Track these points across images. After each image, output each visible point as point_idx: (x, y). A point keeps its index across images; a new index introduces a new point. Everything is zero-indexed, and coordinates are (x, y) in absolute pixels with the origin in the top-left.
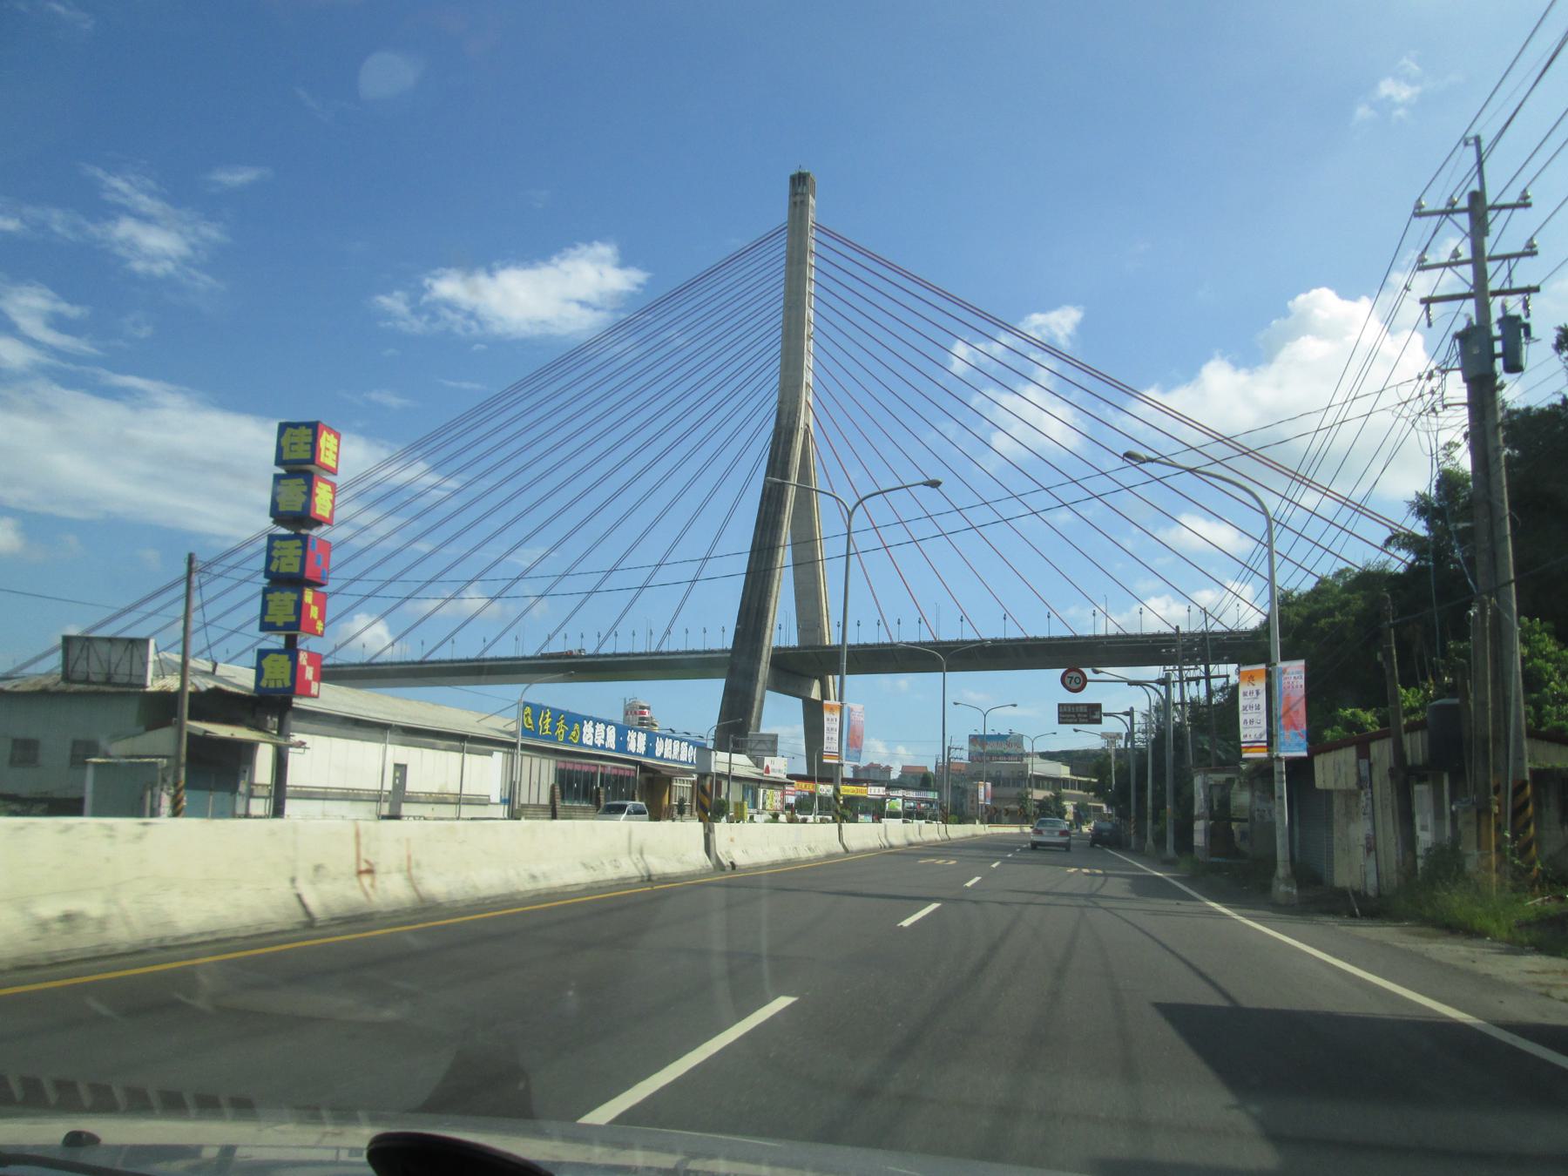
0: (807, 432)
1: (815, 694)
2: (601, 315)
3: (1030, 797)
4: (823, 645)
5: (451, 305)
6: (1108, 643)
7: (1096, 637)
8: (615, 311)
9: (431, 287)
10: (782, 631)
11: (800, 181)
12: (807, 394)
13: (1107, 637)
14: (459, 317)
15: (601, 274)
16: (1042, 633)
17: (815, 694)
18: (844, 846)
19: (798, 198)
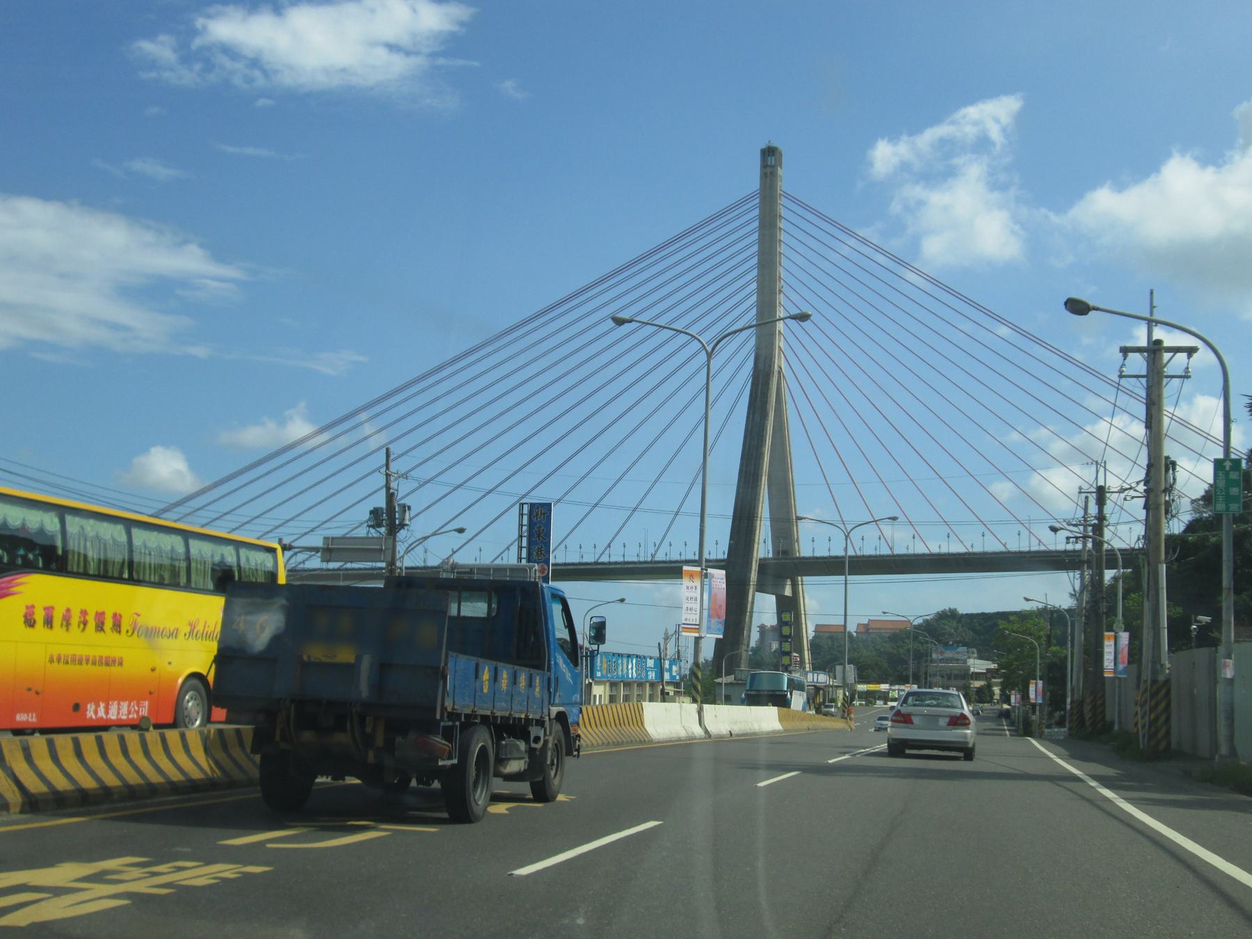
0: (779, 373)
1: (788, 592)
2: (414, 61)
3: (972, 686)
4: (794, 556)
5: (229, 51)
6: (1030, 557)
7: (1021, 553)
8: (433, 55)
9: (205, 28)
10: (763, 547)
11: (770, 154)
12: (780, 340)
13: (1029, 552)
14: (239, 66)
15: (415, 11)
16: (978, 549)
17: (788, 592)
18: (706, 731)
19: (768, 170)
